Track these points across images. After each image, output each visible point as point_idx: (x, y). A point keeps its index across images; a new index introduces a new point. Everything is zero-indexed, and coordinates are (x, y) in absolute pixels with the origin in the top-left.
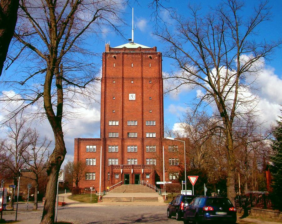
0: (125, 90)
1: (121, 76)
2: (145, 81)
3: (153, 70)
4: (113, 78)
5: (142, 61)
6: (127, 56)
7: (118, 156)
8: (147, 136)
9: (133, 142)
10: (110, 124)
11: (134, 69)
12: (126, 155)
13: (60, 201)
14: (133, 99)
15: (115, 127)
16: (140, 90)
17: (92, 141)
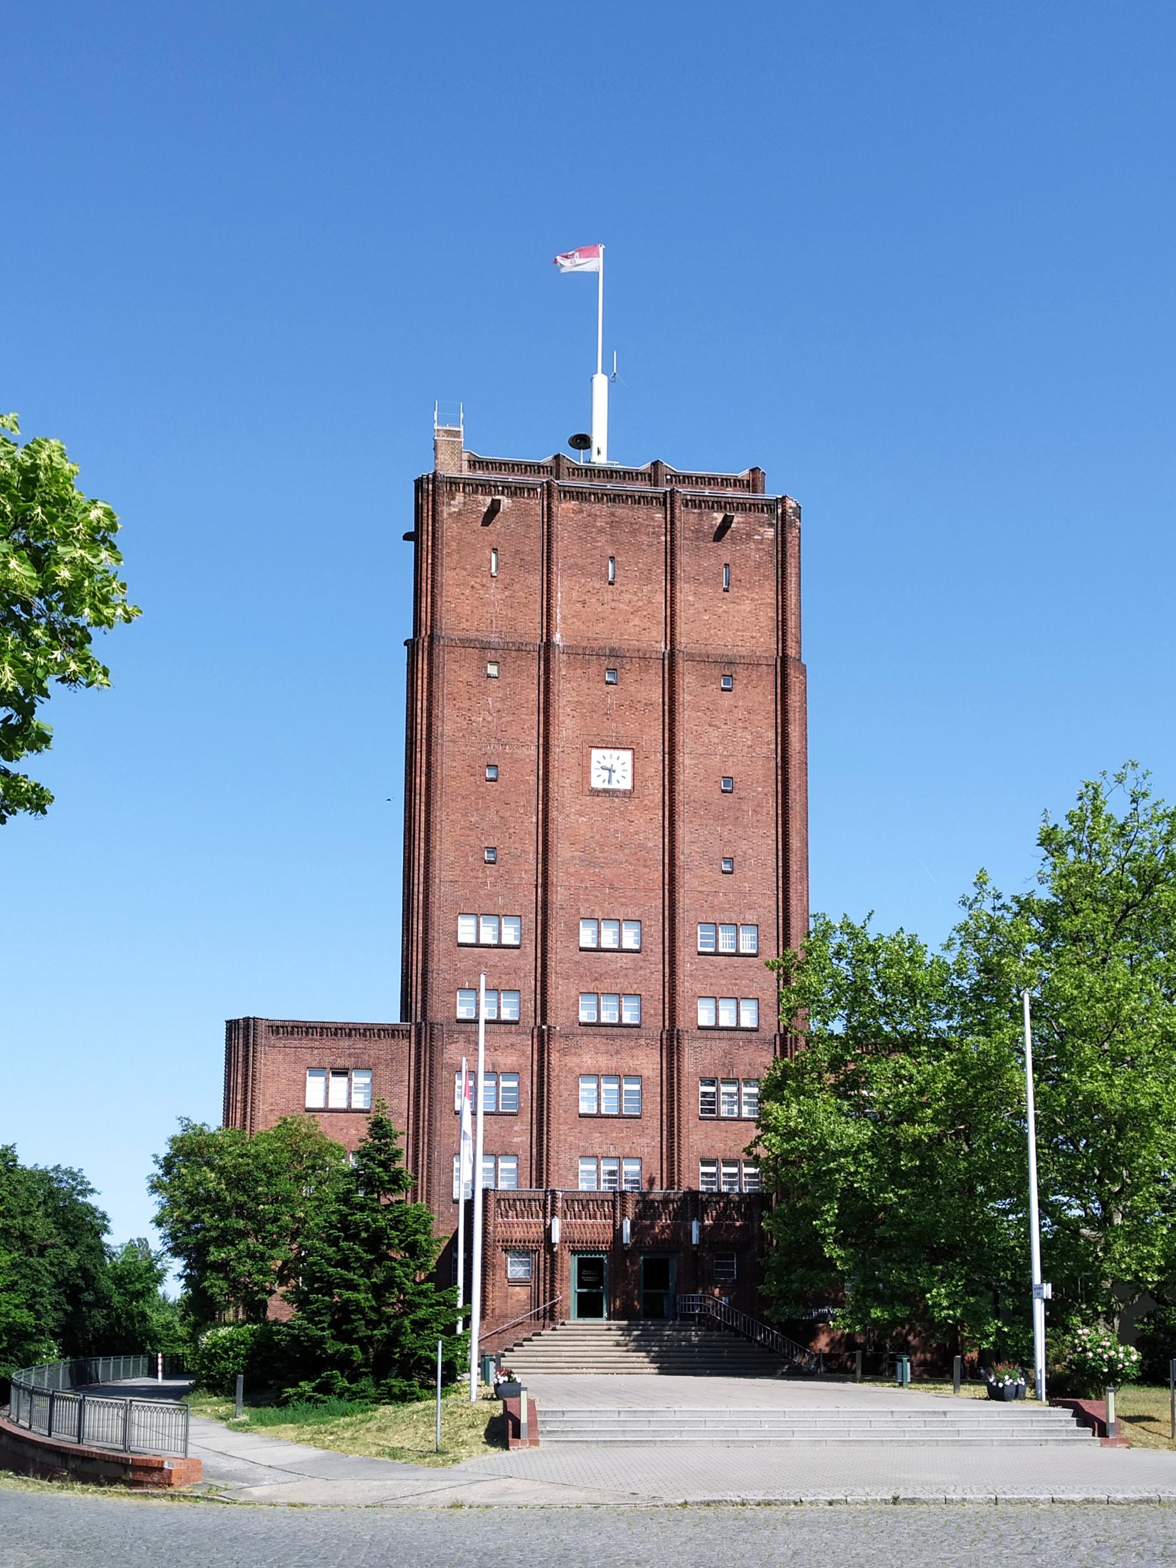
0: (566, 727)
1: (532, 631)
2: (687, 680)
3: (747, 606)
4: (485, 647)
5: (671, 552)
6: (581, 511)
7: (515, 1140)
8: (705, 1017)
9: (617, 1052)
10: (512, 931)
11: (626, 597)
12: (561, 1131)
13: (405, 1042)
14: (614, 786)
15: (527, 1092)
16: (654, 735)
17: (345, 1043)
